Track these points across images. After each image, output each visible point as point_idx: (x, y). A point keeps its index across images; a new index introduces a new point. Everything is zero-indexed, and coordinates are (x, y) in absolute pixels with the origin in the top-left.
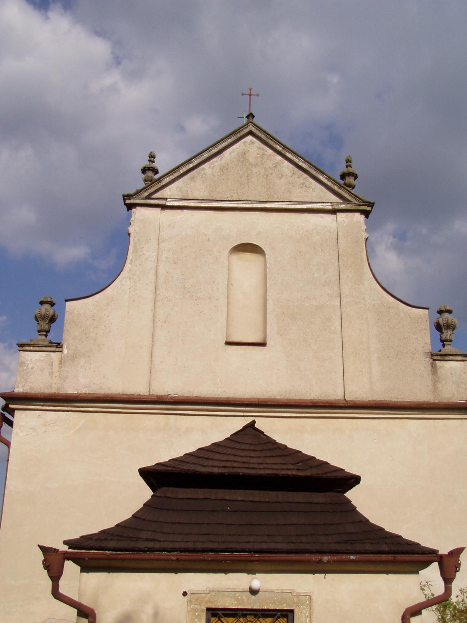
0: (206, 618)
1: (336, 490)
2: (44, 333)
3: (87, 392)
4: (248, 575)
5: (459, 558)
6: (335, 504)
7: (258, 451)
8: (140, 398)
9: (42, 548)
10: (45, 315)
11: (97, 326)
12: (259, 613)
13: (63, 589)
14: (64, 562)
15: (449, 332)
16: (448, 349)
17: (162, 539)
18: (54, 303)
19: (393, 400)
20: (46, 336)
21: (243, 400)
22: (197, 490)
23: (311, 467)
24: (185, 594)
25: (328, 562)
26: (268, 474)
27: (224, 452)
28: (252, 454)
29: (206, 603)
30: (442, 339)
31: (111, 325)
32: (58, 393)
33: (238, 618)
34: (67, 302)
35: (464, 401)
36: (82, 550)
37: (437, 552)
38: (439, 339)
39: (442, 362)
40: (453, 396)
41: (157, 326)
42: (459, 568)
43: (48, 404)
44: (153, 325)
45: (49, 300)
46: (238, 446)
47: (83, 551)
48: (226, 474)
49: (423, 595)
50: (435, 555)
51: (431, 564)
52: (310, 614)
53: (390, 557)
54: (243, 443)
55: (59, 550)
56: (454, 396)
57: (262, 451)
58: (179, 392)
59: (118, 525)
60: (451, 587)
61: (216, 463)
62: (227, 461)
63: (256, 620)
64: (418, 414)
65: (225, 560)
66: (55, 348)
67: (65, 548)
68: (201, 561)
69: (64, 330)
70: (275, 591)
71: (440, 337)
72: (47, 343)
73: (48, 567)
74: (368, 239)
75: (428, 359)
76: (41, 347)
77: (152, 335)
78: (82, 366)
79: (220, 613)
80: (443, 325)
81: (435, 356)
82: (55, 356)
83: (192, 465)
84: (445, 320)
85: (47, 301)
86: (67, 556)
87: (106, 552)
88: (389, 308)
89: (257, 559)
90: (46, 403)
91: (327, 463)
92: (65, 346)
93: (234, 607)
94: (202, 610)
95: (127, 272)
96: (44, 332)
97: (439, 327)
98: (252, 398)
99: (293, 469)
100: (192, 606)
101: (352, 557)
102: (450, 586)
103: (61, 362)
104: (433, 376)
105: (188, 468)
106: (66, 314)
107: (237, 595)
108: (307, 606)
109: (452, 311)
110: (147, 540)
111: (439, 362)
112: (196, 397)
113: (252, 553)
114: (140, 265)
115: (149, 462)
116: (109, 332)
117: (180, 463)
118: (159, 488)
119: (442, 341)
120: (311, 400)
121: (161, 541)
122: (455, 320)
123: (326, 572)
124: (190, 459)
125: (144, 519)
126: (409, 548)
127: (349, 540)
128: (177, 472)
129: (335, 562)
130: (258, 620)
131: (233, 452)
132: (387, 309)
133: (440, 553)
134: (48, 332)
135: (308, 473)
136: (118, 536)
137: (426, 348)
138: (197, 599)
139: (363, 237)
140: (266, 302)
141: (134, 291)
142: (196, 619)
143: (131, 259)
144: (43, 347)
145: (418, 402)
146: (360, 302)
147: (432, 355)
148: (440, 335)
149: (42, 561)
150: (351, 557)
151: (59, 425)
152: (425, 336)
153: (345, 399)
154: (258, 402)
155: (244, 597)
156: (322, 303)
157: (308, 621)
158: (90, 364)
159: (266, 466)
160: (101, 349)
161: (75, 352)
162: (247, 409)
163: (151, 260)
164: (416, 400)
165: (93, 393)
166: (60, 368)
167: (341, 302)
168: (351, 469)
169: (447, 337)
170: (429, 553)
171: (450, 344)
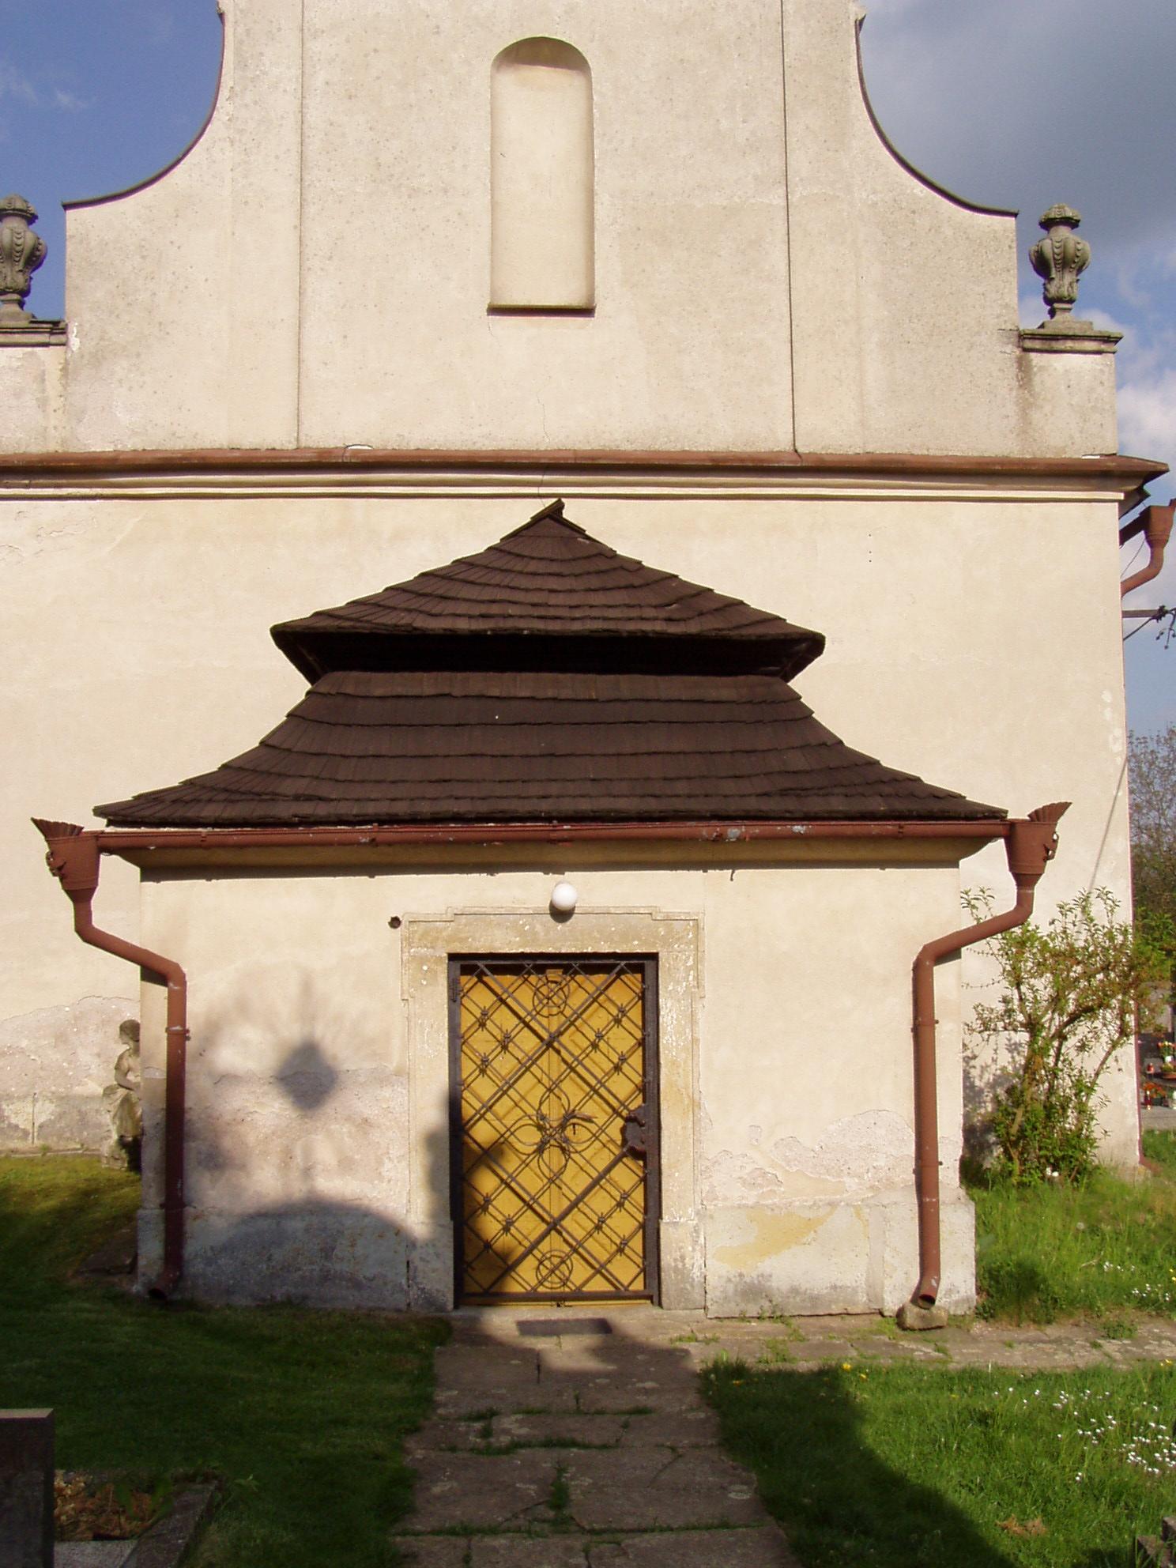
0: (448, 977)
1: (763, 669)
2: (16, 297)
3: (140, 447)
4: (547, 876)
5: (1054, 828)
6: (761, 703)
7: (569, 575)
8: (276, 458)
9: (43, 826)
10: (12, 248)
11: (152, 273)
12: (576, 964)
13: (102, 919)
14: (99, 857)
15: (1068, 277)
16: (1065, 321)
17: (333, 796)
18: (32, 214)
19: (917, 452)
20: (21, 304)
21: (535, 455)
22: (418, 675)
23: (701, 614)
24: (395, 922)
25: (740, 840)
26: (592, 631)
27: (482, 580)
28: (553, 583)
29: (449, 940)
30: (1049, 296)
31: (190, 270)
32: (65, 453)
33: (526, 976)
34: (67, 212)
35: (1098, 457)
36: (140, 827)
37: (1004, 815)
38: (1042, 296)
39: (1046, 355)
40: (1070, 443)
41: (309, 269)
42: (1054, 852)
43: (41, 481)
44: (301, 266)
45: (19, 205)
46: (519, 566)
47: (143, 829)
48: (489, 633)
49: (972, 918)
50: (998, 821)
51: (986, 844)
52: (697, 962)
53: (890, 827)
54: (533, 558)
55: (84, 830)
56: (1073, 443)
57: (580, 575)
58: (373, 440)
59: (225, 767)
60: (1033, 894)
61: (462, 608)
62: (493, 602)
63: (568, 978)
64: (972, 489)
65: (490, 841)
66: (47, 335)
67: (100, 825)
68: (428, 843)
69: (67, 285)
70: (613, 911)
71: (1043, 290)
72: (24, 323)
73: (60, 869)
74: (865, 20)
75: (1009, 348)
76: (11, 333)
77: (298, 294)
78: (120, 381)
79: (481, 964)
80: (1054, 259)
81: (1030, 338)
82: (49, 357)
83: (403, 614)
84: (1058, 245)
85: (14, 210)
86: (103, 845)
87: (199, 830)
88: (914, 212)
89: (566, 835)
90: (35, 479)
91: (741, 603)
92: (73, 329)
93: (514, 951)
94: (440, 959)
95: (223, 123)
96: (13, 292)
97: (1041, 265)
98: (560, 450)
99: (656, 619)
100: (412, 950)
101: (798, 828)
102: (1030, 892)
103: (65, 369)
104: (1021, 391)
105: (394, 621)
106: (68, 243)
107: (521, 922)
108: (689, 943)
109: (1078, 221)
110: (297, 798)
111: (1039, 355)
112: (418, 449)
113: (555, 822)
114: (256, 103)
115: (297, 610)
116: (186, 287)
117: (373, 610)
118: (326, 673)
119: (1049, 301)
120: (709, 452)
121: (332, 800)
122: (1086, 246)
123: (734, 864)
124: (400, 600)
125: (289, 750)
126: (936, 806)
127: (791, 789)
128: (367, 631)
129: (755, 839)
130: (573, 978)
131: (508, 580)
132: (907, 216)
133: (1010, 817)
134: (25, 293)
135: (693, 628)
136: (226, 790)
137: (1006, 318)
138: (425, 934)
139: (851, 17)
140: (593, 198)
141: (246, 177)
142: (425, 979)
143: (232, 88)
144: (14, 333)
145: (980, 457)
146: (838, 197)
147: (1022, 336)
148: (1044, 284)
149: (44, 856)
150: (796, 827)
151: (73, 534)
152: (1005, 287)
153: (796, 451)
154: (575, 459)
155: (538, 927)
156: (738, 200)
157: (691, 978)
158: (142, 375)
159: (588, 612)
160: (168, 333)
161: (101, 343)
162: (547, 478)
163: (285, 91)
164: (976, 454)
165: (154, 448)
166: (65, 386)
167: (789, 197)
168: (799, 617)
169: (1062, 289)
170: (985, 818)
171: (1070, 309)
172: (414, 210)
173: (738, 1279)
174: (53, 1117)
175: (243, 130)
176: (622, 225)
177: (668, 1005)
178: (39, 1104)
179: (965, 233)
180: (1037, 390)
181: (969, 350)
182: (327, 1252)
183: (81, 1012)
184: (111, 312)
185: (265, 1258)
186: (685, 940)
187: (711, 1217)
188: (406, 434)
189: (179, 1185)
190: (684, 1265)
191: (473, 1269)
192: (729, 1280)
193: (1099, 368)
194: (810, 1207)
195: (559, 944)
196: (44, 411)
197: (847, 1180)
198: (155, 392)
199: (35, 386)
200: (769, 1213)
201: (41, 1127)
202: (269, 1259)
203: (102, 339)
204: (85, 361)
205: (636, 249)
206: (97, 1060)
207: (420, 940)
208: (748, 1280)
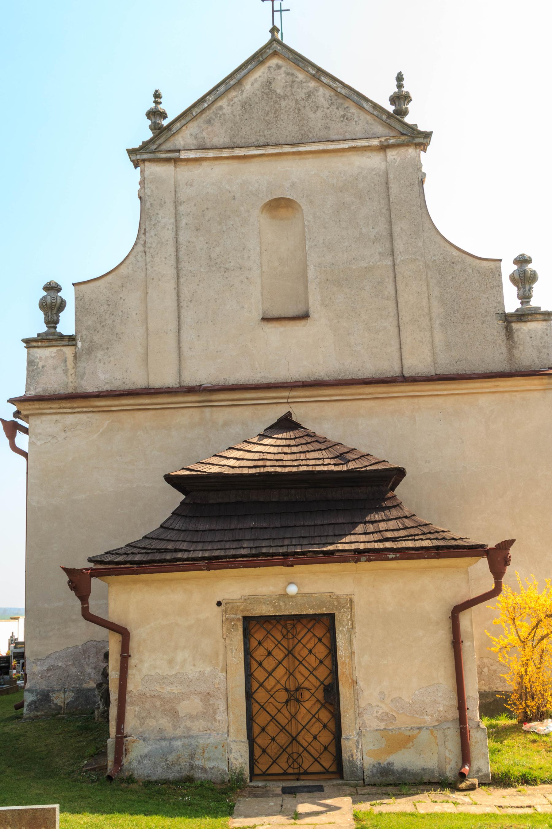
3: (109, 389)
24: (219, 604)
56: (534, 364)
78: (100, 360)
84: (521, 273)
88: (453, 263)
94: (238, 620)
103: (75, 357)
112: (233, 385)
114: (155, 235)
142: (233, 628)
146: (417, 259)
152: (498, 294)
156: (372, 264)
157: (349, 624)
158: (109, 357)
160: (120, 338)
163: (168, 229)
165: (116, 389)
172: (227, 278)
173: (378, 765)
174: (73, 699)
175: (150, 247)
176: (320, 278)
177: (340, 637)
178: (67, 694)
179: (477, 270)
180: (516, 339)
181: (482, 324)
182: (192, 756)
183: (87, 648)
184: (95, 330)
185: (164, 760)
186: (346, 607)
187: (364, 735)
188: (227, 378)
189: (122, 727)
190: (353, 759)
191: (258, 763)
192: (374, 766)
193: (545, 327)
194: (409, 730)
195: (291, 611)
196: (66, 375)
197: (426, 717)
198: (115, 365)
199: (62, 364)
200: (390, 733)
201: (67, 704)
202: (166, 760)
203: (91, 342)
204: (84, 352)
205: (327, 289)
206: (94, 671)
207: (230, 611)
208: (382, 765)
